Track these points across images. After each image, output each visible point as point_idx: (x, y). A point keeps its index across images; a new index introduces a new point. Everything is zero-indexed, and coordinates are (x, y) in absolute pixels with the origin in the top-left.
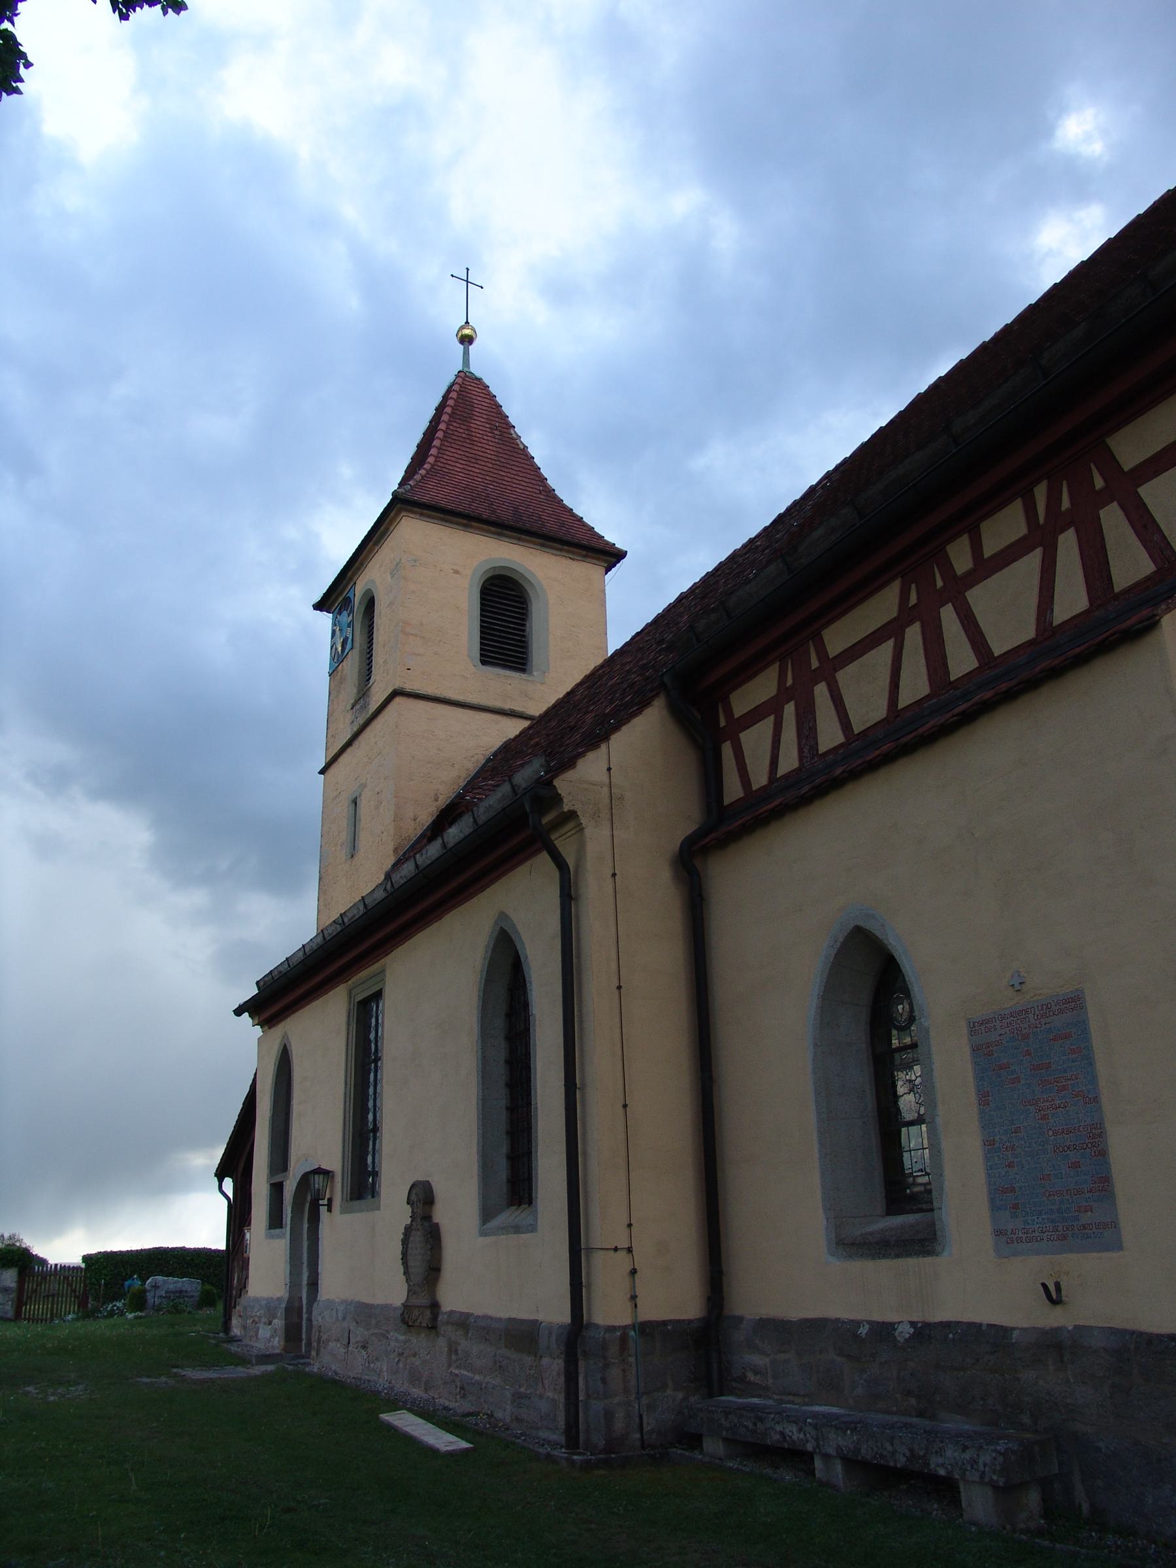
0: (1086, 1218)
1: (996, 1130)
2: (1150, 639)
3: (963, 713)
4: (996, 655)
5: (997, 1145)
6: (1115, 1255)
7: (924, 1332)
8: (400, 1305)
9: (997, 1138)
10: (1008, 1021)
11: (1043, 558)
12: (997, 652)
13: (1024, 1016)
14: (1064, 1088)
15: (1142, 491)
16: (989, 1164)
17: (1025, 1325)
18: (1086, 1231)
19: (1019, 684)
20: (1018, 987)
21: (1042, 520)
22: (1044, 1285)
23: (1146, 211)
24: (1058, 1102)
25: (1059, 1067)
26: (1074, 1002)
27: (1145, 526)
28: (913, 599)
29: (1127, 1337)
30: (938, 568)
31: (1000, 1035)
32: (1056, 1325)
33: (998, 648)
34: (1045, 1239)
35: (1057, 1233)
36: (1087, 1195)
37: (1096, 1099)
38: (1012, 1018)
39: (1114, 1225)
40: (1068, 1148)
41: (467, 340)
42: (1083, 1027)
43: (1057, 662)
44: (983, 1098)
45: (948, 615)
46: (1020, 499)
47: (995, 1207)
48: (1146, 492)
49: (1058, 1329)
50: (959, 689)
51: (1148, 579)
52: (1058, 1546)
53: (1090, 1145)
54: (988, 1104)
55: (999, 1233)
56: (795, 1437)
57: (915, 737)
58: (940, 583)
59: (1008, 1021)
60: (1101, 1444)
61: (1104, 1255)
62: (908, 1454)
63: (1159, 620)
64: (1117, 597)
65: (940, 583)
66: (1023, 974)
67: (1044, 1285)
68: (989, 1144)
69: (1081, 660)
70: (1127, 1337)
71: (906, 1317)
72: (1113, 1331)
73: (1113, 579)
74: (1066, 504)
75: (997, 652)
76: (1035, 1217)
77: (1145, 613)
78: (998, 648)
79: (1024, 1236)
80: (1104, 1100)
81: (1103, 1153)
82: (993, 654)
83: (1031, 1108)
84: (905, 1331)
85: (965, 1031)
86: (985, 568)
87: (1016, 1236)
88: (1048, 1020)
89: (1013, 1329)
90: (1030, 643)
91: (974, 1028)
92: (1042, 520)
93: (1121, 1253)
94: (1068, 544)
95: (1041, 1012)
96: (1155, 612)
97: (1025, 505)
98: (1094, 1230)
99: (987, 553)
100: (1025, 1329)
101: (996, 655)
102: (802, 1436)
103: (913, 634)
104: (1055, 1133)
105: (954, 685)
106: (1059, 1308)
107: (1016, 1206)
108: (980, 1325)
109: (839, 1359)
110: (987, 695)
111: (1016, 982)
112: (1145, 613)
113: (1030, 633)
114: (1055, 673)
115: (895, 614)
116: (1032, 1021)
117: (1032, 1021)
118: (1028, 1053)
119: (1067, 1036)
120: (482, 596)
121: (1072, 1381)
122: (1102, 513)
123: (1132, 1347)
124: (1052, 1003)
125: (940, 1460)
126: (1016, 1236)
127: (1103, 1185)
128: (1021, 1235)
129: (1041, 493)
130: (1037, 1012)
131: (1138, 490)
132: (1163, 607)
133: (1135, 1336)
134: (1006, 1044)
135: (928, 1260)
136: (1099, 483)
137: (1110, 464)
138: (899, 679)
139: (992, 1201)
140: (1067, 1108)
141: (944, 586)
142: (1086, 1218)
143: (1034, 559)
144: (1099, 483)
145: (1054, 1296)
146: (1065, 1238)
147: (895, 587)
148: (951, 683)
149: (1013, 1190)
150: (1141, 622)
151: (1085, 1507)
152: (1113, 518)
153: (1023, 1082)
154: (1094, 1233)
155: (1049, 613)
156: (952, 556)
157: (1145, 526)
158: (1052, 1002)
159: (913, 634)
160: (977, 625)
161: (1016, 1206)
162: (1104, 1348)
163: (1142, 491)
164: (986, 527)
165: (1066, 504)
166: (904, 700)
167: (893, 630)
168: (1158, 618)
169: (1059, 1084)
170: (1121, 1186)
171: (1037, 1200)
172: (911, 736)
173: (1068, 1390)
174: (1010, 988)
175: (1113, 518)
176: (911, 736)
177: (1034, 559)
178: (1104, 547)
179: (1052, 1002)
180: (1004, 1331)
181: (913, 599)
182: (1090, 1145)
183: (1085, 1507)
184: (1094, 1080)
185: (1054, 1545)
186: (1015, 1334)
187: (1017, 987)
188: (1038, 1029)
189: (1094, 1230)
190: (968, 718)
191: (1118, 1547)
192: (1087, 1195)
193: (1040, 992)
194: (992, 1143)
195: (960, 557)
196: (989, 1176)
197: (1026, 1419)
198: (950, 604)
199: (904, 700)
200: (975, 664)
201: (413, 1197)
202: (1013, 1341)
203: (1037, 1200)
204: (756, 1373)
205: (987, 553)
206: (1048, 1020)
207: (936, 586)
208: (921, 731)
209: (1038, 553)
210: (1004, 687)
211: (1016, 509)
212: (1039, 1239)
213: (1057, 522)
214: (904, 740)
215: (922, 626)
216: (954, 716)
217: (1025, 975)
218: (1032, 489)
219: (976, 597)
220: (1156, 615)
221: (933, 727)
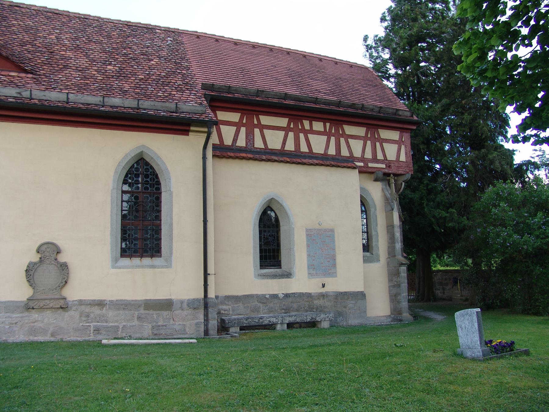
7: (287, 296)
8: (26, 300)
9: (311, 254)
26: (332, 230)
39: (336, 273)
42: (334, 235)
44: (308, 246)
47: (309, 268)
55: (309, 274)
56: (274, 321)
62: (311, 318)
64: (341, 156)
68: (309, 255)
71: (281, 293)
84: (281, 296)
85: (305, 230)
91: (307, 230)
92: (328, 131)
102: (277, 320)
108: (303, 293)
109: (259, 304)
119: (330, 237)
120: (413, 141)
125: (319, 318)
127: (334, 265)
135: (289, 279)
146: (325, 275)
161: (314, 269)
180: (310, 294)
184: (335, 246)
197: (315, 310)
201: (43, 248)
204: (225, 311)
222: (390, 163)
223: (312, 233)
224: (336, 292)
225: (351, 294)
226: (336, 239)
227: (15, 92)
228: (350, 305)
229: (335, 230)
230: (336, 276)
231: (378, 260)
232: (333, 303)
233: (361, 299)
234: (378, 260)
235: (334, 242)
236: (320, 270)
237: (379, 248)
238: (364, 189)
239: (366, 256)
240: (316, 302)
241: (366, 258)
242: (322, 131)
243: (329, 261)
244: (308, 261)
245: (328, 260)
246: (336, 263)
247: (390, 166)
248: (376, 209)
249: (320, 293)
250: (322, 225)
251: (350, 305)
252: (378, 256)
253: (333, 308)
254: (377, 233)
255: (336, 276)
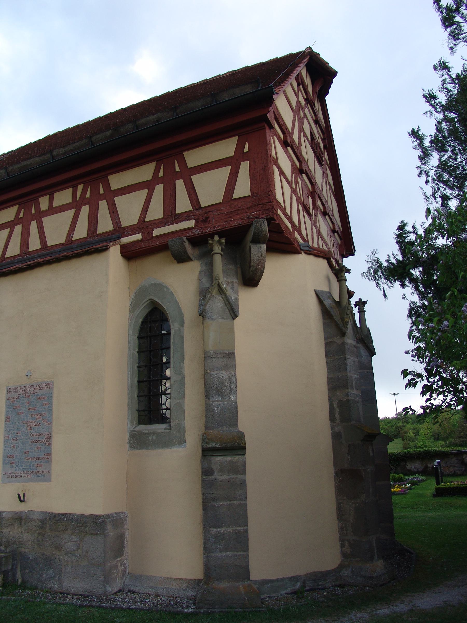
0: (39, 469)
1: (10, 432)
2: (104, 254)
3: (29, 265)
4: (48, 246)
5: (9, 438)
6: (48, 483)
9: (10, 435)
10: (23, 389)
11: (75, 213)
12: (49, 244)
13: (29, 388)
14: (39, 418)
15: (193, 177)
16: (5, 445)
17: (9, 511)
18: (39, 474)
19: (53, 259)
20: (29, 377)
21: (78, 199)
22: (19, 495)
23: (267, 61)
24: (36, 423)
25: (39, 410)
26: (49, 385)
27: (113, 212)
28: (21, 215)
29: (47, 514)
30: (34, 206)
31: (19, 395)
32: (21, 510)
33: (50, 243)
34: (22, 477)
35: (28, 474)
36: (41, 460)
37: (51, 424)
38: (25, 389)
39: (49, 472)
40: (37, 441)
43: (69, 254)
44: (8, 419)
45: (34, 225)
46: (72, 188)
47: (4, 463)
48: (194, 178)
49: (21, 512)
50: (31, 255)
51: (110, 232)
52: (3, 597)
53: (45, 441)
54: (9, 422)
55: (4, 473)
57: (8, 270)
58: (33, 212)
59: (23, 389)
60: (30, 556)
61: (44, 483)
63: (109, 248)
64: (97, 235)
65: (33, 212)
66: (32, 372)
67: (19, 495)
69: (78, 256)
70: (47, 514)
72: (42, 512)
73: (98, 229)
74: (88, 195)
75: (49, 244)
76: (20, 468)
77: (105, 244)
78: (50, 243)
79: (14, 475)
80: (54, 424)
81: (50, 444)
82: (47, 245)
83: (26, 425)
86: (52, 210)
87: (12, 475)
88: (38, 391)
89: (4, 512)
90: (62, 244)
91: (9, 390)
92: (78, 199)
93: (50, 483)
94: (85, 210)
95: (36, 388)
96: (109, 245)
97: (50, 198)
98: (42, 474)
99: (55, 205)
100: (9, 512)
101: (48, 246)
103: (18, 229)
104: (33, 435)
105: (29, 253)
106: (23, 503)
107: (13, 463)
110: (40, 260)
111: (29, 374)
112: (105, 244)
113: (63, 240)
114: (68, 258)
115: (13, 219)
116: (32, 391)
117: (32, 391)
118: (28, 403)
121: (23, 532)
122: (100, 203)
123: (48, 519)
124: (41, 385)
126: (12, 475)
127: (48, 456)
128: (13, 475)
129: (80, 188)
130: (35, 388)
131: (114, 198)
132: (112, 243)
133: (50, 514)
134: (20, 399)
136: (102, 191)
137: (107, 185)
138: (8, 245)
139: (4, 461)
140: (39, 426)
141: (35, 213)
142: (39, 469)
143: (71, 213)
144: (102, 191)
145: (22, 499)
147: (16, 208)
148: (28, 252)
149: (13, 457)
150: (103, 247)
151: (20, 581)
152: (103, 206)
153: (24, 414)
154: (41, 475)
155: (72, 235)
156: (40, 202)
157: (113, 212)
158: (41, 384)
159: (18, 229)
160: (44, 232)
162: (37, 519)
163: (193, 177)
164: (57, 195)
165: (88, 195)
166: (8, 254)
167: (11, 225)
168: (109, 247)
169: (38, 416)
170: (54, 457)
171: (22, 461)
172: (7, 269)
173: (21, 536)
174: (26, 377)
175: (103, 206)
176: (7, 269)
177: (71, 213)
178: (97, 215)
179: (41, 384)
181: (21, 215)
182: (45, 441)
183: (20, 581)
184: (51, 416)
185: (2, 597)
186: (4, 514)
187: (29, 376)
188: (34, 394)
189: (42, 474)
190: (31, 267)
191: (29, 594)
192: (41, 460)
193: (37, 380)
194: (8, 437)
195: (44, 203)
196: (4, 450)
198: (35, 221)
199: (8, 254)
200: (40, 247)
202: (3, 517)
203: (22, 461)
205: (55, 205)
206: (38, 391)
207: (32, 212)
208: (11, 268)
209: (73, 211)
210: (48, 258)
211: (69, 192)
212: (20, 476)
213: (83, 201)
214: (4, 270)
215: (22, 227)
216: (26, 265)
217: (33, 372)
218: (77, 186)
219: (46, 221)
220: (109, 246)
221: (16, 268)
222: (208, 213)
223: (16, 395)
224: (47, 512)
225: (72, 520)
226: (55, 402)
227: (462, 302)
228: (70, 546)
229: (55, 386)
230: (50, 480)
231: (182, 441)
232: (36, 535)
233: (92, 534)
234: (182, 441)
235: (50, 407)
236: (22, 466)
237: (184, 410)
238: (160, 285)
239: (153, 433)
240: (6, 530)
241: (154, 437)
242: (106, 205)
243: (39, 448)
244: (5, 447)
245: (38, 445)
246: (51, 451)
247: (207, 218)
248: (182, 324)
249: (16, 513)
250: (31, 377)
251: (70, 546)
252: (181, 430)
253: (36, 546)
254: (183, 377)
255: (50, 480)
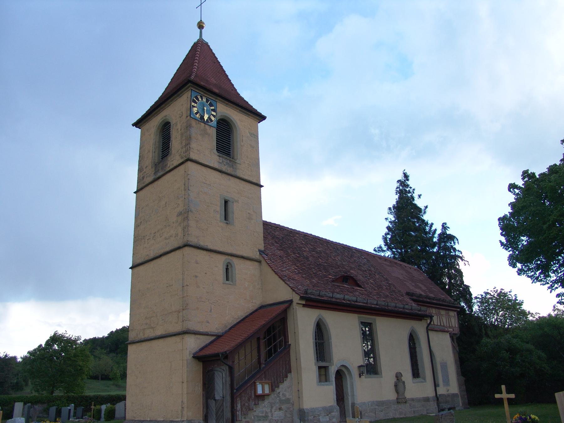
41: (201, 26)
